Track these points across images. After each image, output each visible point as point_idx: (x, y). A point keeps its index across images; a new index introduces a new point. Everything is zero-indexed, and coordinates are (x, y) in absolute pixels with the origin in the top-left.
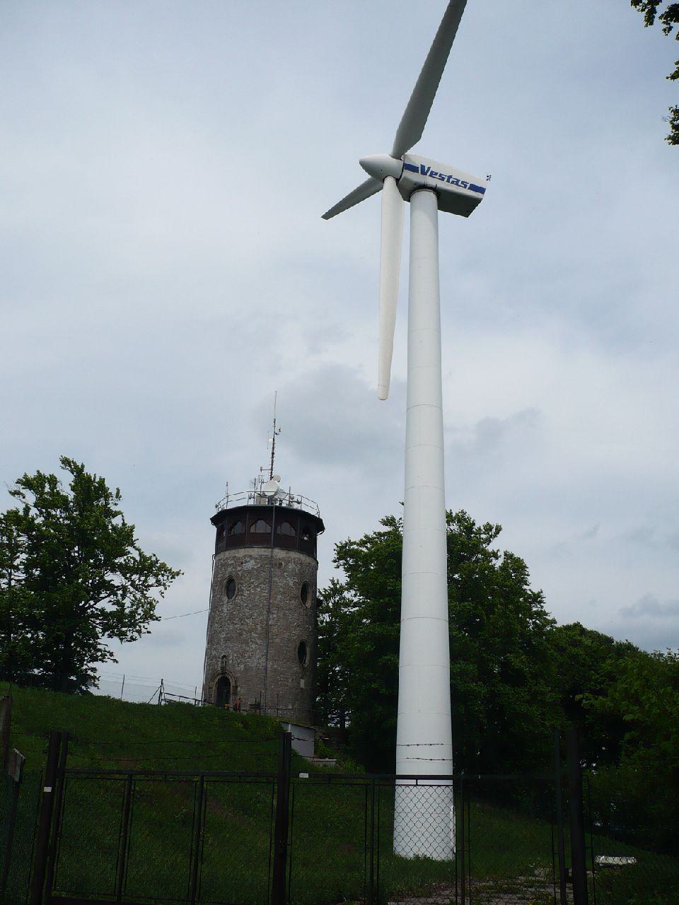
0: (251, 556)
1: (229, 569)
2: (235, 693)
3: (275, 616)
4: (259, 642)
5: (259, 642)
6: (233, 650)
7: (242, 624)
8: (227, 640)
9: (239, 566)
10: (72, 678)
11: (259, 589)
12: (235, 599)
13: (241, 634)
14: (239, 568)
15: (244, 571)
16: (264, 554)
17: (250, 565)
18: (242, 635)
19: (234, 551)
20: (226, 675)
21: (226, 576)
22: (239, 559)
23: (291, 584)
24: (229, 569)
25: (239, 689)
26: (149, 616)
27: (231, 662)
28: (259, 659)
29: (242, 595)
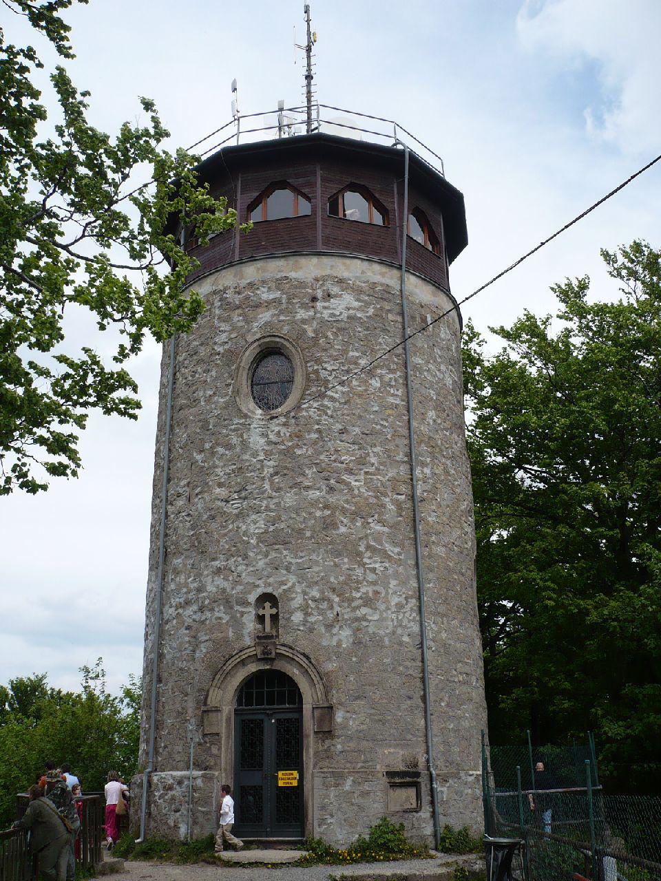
0: (341, 281)
1: (265, 316)
2: (326, 733)
3: (427, 471)
4: (392, 550)
5: (392, 550)
6: (302, 578)
7: (331, 489)
8: (273, 540)
9: (304, 306)
10: (505, 603)
11: (376, 383)
12: (298, 407)
13: (329, 525)
14: (302, 314)
15: (323, 322)
16: (384, 281)
17: (343, 305)
18: (335, 526)
19: (281, 263)
20: (280, 665)
21: (250, 339)
22: (302, 285)
23: (449, 382)
24: (265, 316)
25: (339, 716)
26: (637, 247)
27: (297, 617)
28: (400, 606)
29: (322, 396)
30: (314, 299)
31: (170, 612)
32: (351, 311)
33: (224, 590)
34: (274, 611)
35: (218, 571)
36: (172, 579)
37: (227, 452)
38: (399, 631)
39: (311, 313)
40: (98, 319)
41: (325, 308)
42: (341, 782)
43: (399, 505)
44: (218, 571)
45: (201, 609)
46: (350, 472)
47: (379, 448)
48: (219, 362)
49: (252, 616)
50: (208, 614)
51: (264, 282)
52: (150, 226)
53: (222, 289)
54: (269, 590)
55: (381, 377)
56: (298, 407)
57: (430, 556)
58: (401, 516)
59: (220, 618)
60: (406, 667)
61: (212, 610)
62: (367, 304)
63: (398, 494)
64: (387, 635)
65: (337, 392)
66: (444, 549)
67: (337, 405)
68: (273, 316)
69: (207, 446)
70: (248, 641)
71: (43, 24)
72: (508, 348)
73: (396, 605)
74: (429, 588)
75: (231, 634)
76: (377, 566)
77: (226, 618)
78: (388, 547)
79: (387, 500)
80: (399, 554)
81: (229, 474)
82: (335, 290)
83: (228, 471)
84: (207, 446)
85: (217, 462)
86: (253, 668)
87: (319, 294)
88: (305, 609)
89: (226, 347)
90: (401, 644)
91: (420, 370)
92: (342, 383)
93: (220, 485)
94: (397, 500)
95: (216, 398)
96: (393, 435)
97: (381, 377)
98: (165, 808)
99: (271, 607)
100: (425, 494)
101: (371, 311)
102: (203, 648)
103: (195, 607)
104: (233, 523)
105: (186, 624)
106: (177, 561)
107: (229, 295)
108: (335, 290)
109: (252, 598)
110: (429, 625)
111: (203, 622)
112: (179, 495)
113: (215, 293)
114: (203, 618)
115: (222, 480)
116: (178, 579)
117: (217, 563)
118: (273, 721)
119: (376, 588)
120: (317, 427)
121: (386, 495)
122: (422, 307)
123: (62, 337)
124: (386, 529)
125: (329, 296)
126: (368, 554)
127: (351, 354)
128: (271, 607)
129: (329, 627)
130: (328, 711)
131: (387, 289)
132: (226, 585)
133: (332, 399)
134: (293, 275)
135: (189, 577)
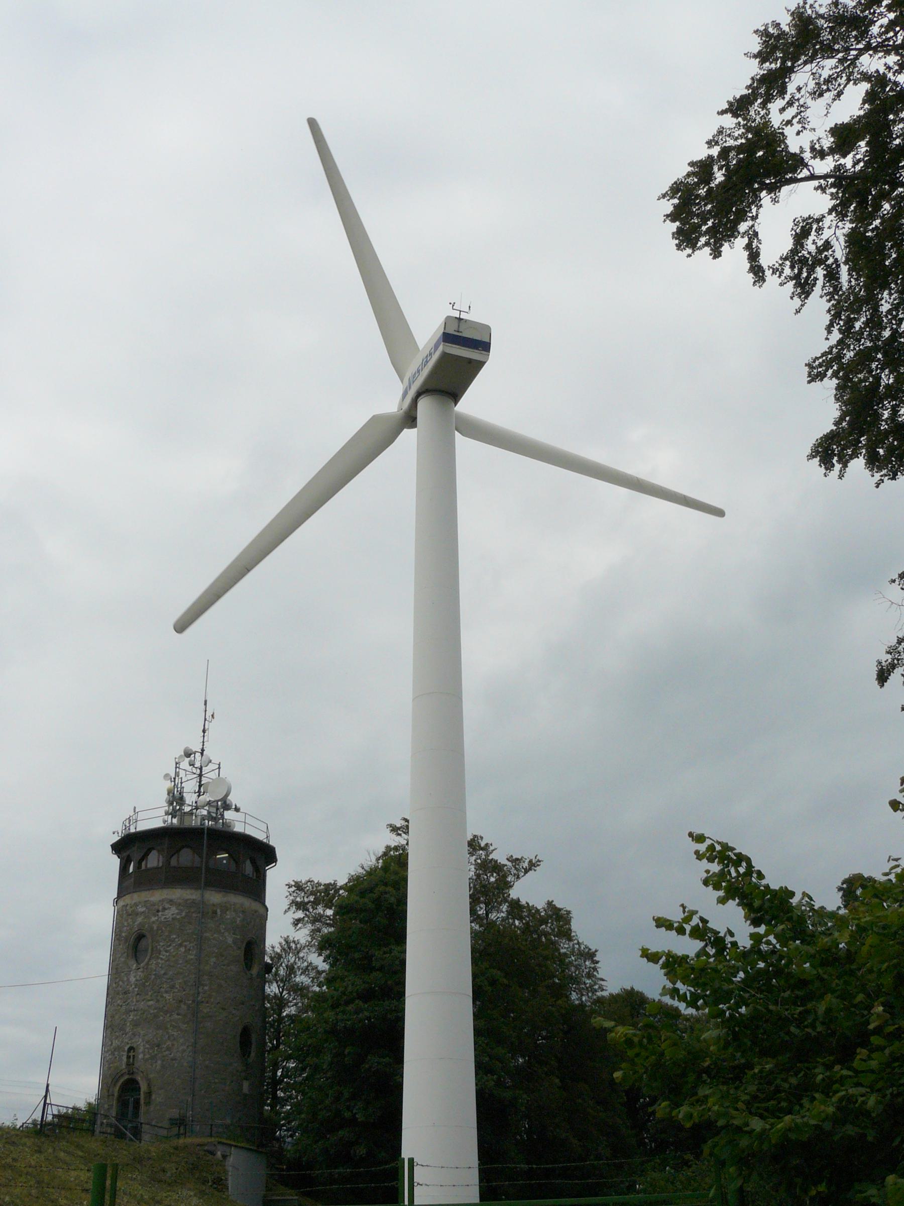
0: (171, 901)
1: (140, 919)
11: (183, 949)
14: (154, 919)
21: (134, 931)
24: (140, 919)
27: (141, 1056)
28: (184, 1051)
29: (158, 958)
30: (158, 911)
34: (134, 1054)
39: (156, 918)
40: (824, 471)
41: (162, 915)
46: (166, 992)
49: (126, 1056)
51: (140, 902)
52: (865, 11)
54: (132, 1045)
55: (186, 946)
56: (147, 964)
62: (182, 911)
65: (164, 955)
67: (163, 961)
68: (143, 919)
70: (124, 1067)
72: (895, 863)
76: (175, 1033)
82: (167, 906)
86: (126, 1077)
87: (160, 908)
88: (143, 1052)
92: (166, 951)
97: (186, 946)
101: (184, 914)
108: (167, 906)
109: (126, 1049)
120: (154, 973)
130: (149, 1094)
131: (193, 902)
133: (162, 959)
134: (152, 899)
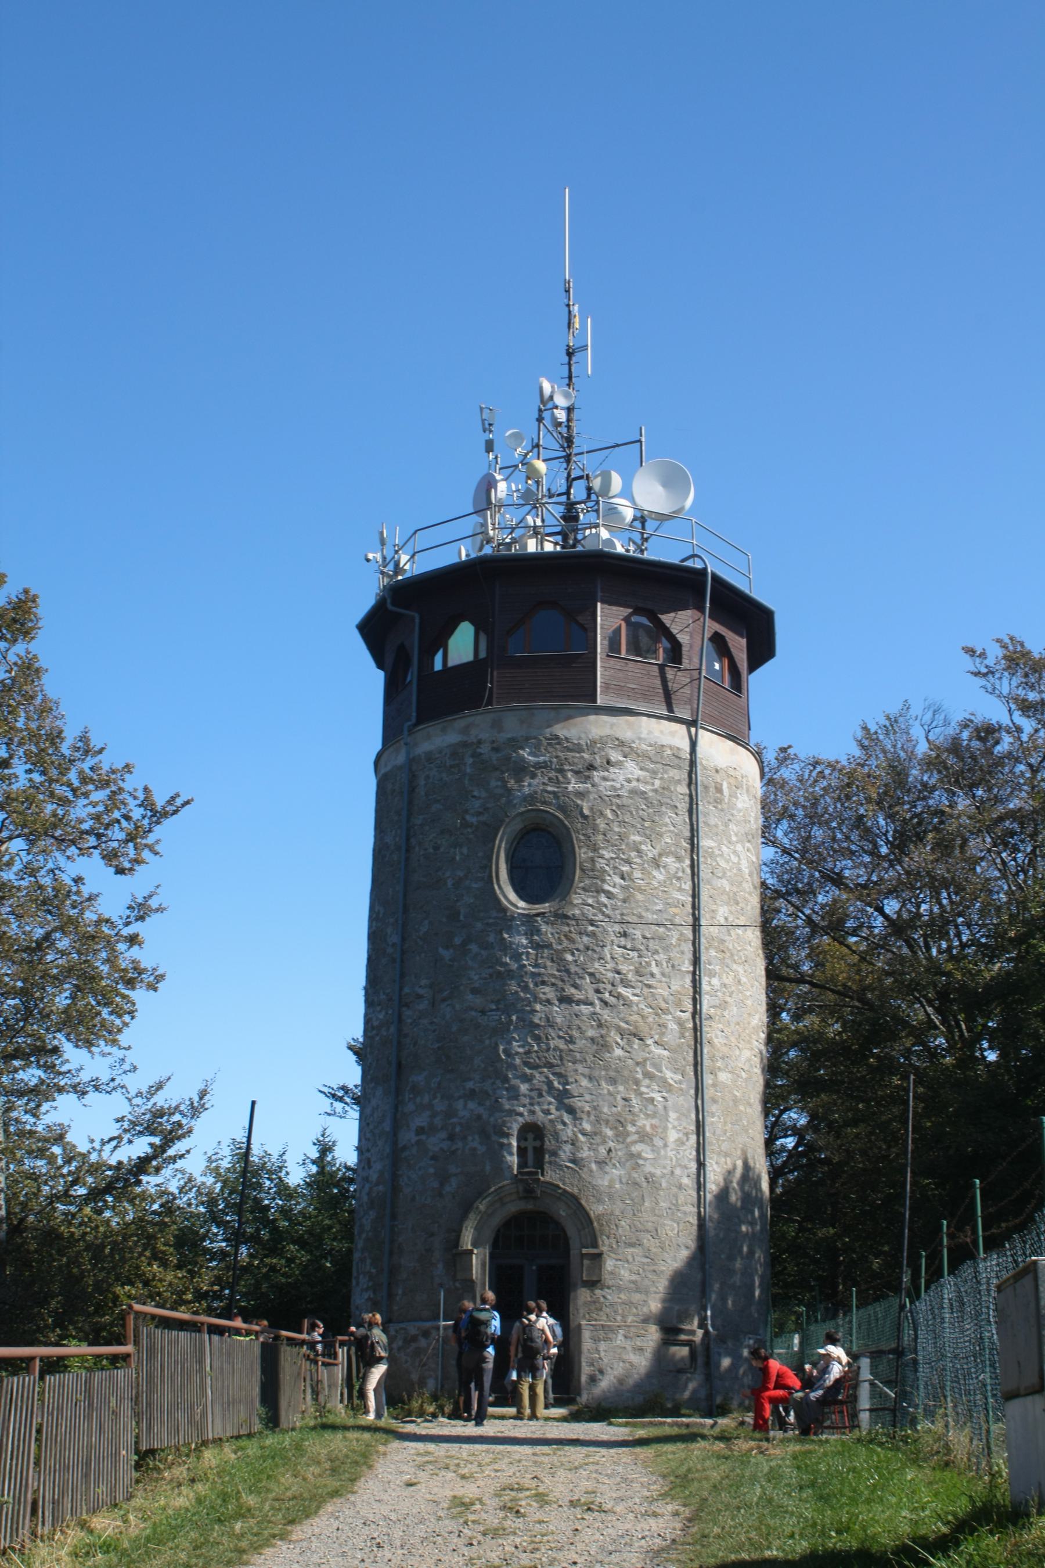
3: (715, 981)
31: (408, 1136)
32: (634, 784)
33: (479, 1117)
34: (538, 1144)
35: (472, 1094)
36: (410, 1099)
37: (483, 952)
38: (678, 1171)
41: (605, 779)
42: (610, 1335)
43: (680, 1023)
44: (472, 1094)
45: (451, 1137)
47: (662, 956)
48: (471, 836)
50: (460, 1144)
53: (475, 741)
57: (714, 1085)
58: (684, 1037)
59: (475, 1149)
60: (685, 1213)
61: (464, 1138)
63: (682, 1011)
64: (663, 1176)
66: (729, 1075)
69: (457, 941)
71: (789, 1133)
73: (676, 1141)
74: (712, 1123)
75: (488, 1168)
77: (481, 1149)
78: (669, 1075)
79: (670, 1017)
80: (680, 1082)
81: (485, 979)
83: (484, 975)
84: (457, 941)
85: (470, 963)
89: (482, 818)
90: (680, 1187)
91: (712, 856)
93: (475, 991)
94: (680, 1018)
95: (467, 882)
96: (679, 939)
98: (406, 1362)
99: (535, 1140)
100: (712, 1010)
102: (454, 1182)
103: (443, 1135)
104: (490, 1038)
105: (431, 1154)
106: (418, 1078)
107: (485, 749)
110: (712, 1165)
111: (453, 1152)
112: (420, 997)
113: (465, 745)
114: (454, 1148)
115: (477, 985)
116: (418, 1100)
117: (470, 1085)
118: (534, 1268)
119: (654, 1121)
121: (665, 1011)
122: (717, 771)
123: (26, 591)
124: (666, 1053)
125: (608, 763)
126: (647, 1082)
127: (633, 838)
128: (535, 1140)
129: (601, 1163)
132: (481, 1110)
135: (435, 1098)
